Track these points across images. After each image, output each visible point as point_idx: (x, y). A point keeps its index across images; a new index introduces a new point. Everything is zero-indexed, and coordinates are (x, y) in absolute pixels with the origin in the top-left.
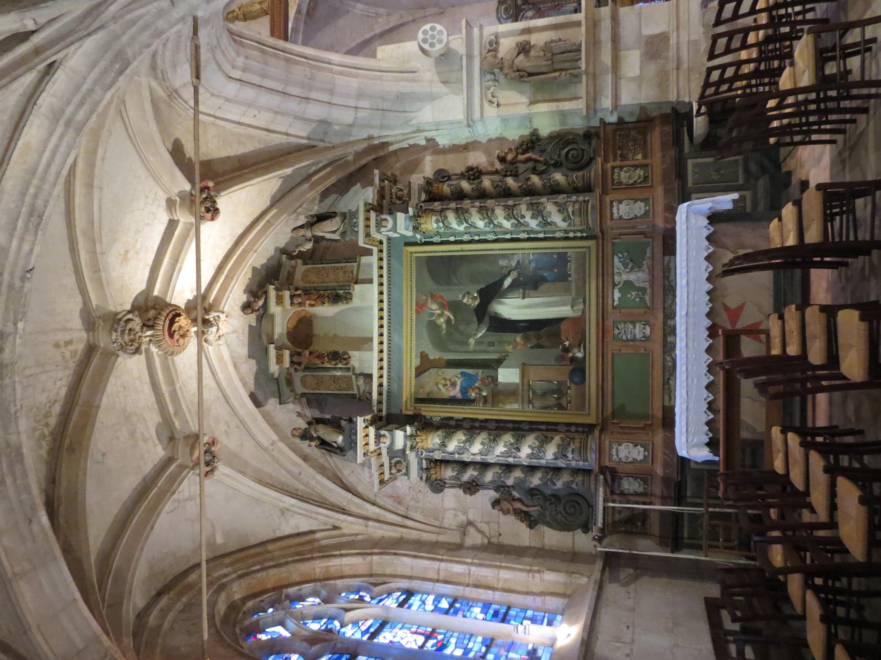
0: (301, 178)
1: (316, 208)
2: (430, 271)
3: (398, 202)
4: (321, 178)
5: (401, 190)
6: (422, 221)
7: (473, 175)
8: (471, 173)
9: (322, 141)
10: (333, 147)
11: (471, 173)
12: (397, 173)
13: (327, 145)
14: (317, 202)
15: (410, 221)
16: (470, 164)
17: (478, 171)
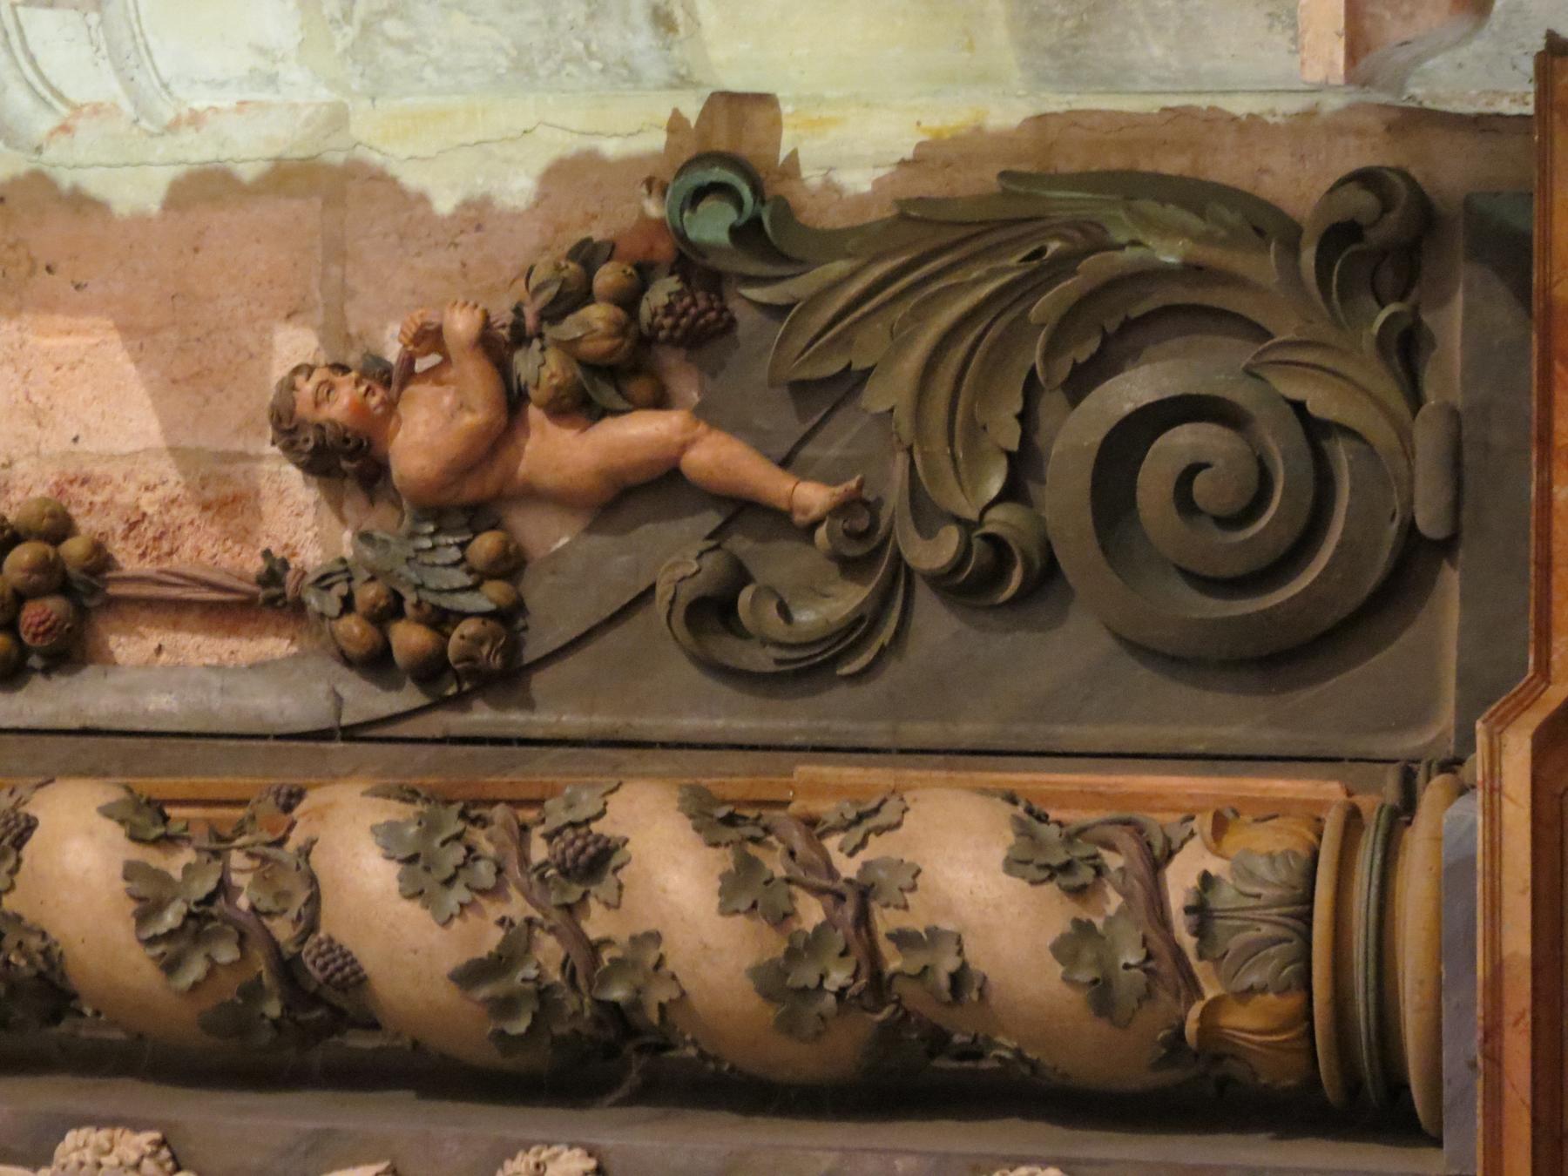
17: (54, 579)
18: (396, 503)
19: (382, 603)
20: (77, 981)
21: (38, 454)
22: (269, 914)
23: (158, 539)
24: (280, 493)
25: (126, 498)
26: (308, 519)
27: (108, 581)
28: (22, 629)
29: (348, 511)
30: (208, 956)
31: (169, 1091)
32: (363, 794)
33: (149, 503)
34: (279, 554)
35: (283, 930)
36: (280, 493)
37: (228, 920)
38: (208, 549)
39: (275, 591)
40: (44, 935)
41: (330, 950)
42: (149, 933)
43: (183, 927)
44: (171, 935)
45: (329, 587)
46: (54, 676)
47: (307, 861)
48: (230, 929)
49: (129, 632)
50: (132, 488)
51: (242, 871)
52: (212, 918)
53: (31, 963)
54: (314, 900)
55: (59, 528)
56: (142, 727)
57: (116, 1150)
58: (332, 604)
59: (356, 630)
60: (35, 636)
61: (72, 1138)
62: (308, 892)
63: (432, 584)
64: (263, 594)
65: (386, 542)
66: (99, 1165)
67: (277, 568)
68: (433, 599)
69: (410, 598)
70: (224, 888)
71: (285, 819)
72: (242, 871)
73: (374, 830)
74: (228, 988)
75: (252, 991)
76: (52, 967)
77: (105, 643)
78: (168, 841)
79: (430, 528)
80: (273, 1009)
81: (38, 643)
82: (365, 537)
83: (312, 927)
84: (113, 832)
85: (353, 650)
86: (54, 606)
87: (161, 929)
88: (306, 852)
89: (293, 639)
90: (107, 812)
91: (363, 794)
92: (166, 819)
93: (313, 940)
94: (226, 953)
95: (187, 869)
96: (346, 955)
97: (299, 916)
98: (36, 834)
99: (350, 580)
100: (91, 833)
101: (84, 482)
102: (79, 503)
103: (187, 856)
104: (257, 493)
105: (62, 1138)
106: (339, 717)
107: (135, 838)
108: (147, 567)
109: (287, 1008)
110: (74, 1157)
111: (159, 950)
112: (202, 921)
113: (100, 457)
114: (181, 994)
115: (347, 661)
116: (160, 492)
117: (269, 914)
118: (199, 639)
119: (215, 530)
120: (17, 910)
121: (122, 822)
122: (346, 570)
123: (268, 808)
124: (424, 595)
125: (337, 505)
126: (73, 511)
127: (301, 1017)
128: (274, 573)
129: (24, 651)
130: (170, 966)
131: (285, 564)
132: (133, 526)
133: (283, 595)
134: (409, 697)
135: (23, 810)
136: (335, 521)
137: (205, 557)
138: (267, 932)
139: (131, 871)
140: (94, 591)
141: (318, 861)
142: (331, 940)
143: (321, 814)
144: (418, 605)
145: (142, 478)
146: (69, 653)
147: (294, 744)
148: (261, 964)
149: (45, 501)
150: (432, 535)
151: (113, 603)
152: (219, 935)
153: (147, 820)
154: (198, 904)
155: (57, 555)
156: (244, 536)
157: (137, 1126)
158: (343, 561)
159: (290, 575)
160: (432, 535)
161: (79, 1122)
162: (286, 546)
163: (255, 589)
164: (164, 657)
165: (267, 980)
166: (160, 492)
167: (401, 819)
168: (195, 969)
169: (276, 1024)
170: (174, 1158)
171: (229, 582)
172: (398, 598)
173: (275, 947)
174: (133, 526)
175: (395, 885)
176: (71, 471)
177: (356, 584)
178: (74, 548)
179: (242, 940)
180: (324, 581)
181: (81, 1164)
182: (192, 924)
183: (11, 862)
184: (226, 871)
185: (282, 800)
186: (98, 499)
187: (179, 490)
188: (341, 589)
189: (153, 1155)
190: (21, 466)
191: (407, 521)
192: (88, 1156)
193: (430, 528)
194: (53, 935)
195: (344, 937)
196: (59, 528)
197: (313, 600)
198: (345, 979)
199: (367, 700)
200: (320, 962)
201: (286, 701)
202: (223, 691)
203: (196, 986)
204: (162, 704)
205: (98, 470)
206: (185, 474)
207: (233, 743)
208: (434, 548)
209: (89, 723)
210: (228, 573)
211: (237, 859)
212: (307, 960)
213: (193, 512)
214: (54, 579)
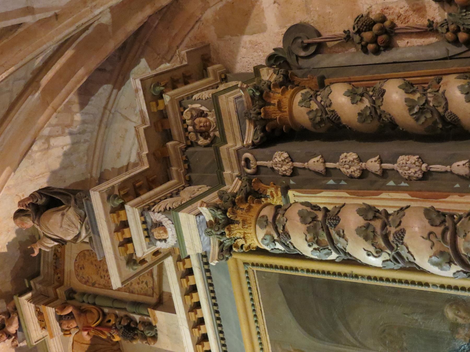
0: (22, 83)
1: (78, 117)
2: (290, 304)
3: (202, 141)
4: (58, 75)
5: (202, 114)
6: (237, 231)
7: (374, 40)
8: (367, 35)
9: (29, 10)
10: (56, 16)
11: (367, 35)
12: (211, 34)
13: (39, 16)
14: (76, 107)
15: (209, 234)
16: (364, 10)
17: (384, 31)
18: (456, 5)
19: (455, 29)
20: (397, 123)
21: (377, 4)
22: (437, 106)
23: (404, 19)
24: (430, 6)
25: (397, 11)
26: (437, 11)
27: (395, 30)
28: (378, 42)
29: (446, 8)
30: (425, 117)
31: (419, 144)
32: (455, 78)
33: (402, 11)
34: (431, 20)
35: (441, 110)
36: (430, 6)
37: (428, 109)
38: (416, 20)
39: (431, 28)
40: (390, 115)
41: (451, 114)
42: (412, 113)
43: (419, 111)
44: (416, 113)
45: (443, 26)
46: (386, 51)
47: (444, 95)
48: (429, 110)
49: (401, 39)
50: (398, 9)
51: (430, 97)
52: (425, 109)
53: (388, 120)
54: (447, 104)
55: (383, 19)
56: (406, 60)
57: (410, 160)
58: (444, 31)
59: (450, 35)
60: (381, 43)
61: (401, 158)
62: (445, 102)
63: (466, 24)
64: (429, 29)
65: (455, 15)
66: (407, 163)
67: (431, 23)
68: (467, 27)
69: (462, 28)
70: (427, 102)
71: (438, 86)
72: (430, 97)
73: (458, 87)
74: (430, 123)
75: (435, 123)
76: (392, 120)
77: (396, 42)
78: (414, 92)
79: (464, 11)
80: (440, 126)
81: (382, 45)
82: (450, 14)
83: (447, 109)
84: (401, 91)
85: (450, 40)
86: (384, 37)
87: (414, 112)
88: (444, 93)
89: (437, 37)
90: (400, 87)
91: (455, 78)
92: (414, 87)
93: (447, 112)
94: (429, 116)
95: (419, 98)
96: (455, 115)
97: (444, 107)
98: (386, 93)
99: (447, 24)
100: (397, 92)
101: (387, 9)
102: (387, 13)
103: (418, 95)
104: (425, 6)
105: (398, 158)
106: (448, 54)
107: (407, 92)
108: (403, 25)
109: (443, 126)
110: (401, 162)
111: (414, 116)
112: (422, 110)
113: (390, 3)
114: (421, 125)
115: (449, 42)
116: (404, 9)
117: (437, 106)
118: (416, 39)
119: (417, 16)
120: (384, 110)
121: (403, 89)
122: (447, 22)
123: (435, 83)
124: (464, 26)
125: (443, 7)
126: (386, 15)
127: (447, 127)
128: (431, 23)
129: (379, 47)
130: (417, 120)
131: (433, 22)
132: (399, 17)
133: (433, 29)
134: (464, 48)
135: (382, 88)
136: (443, 11)
137: (415, 22)
138: (437, 110)
139: (407, 100)
140: (392, 32)
141: (447, 95)
142: (451, 112)
143: (446, 84)
144: (464, 28)
145: (400, 6)
146: (389, 46)
147: (439, 61)
148: (436, 117)
149: (379, 14)
150: (465, 12)
151: (396, 34)
152: (427, 112)
153: (409, 87)
154: (421, 106)
155: (384, 26)
156: (423, 16)
157: (414, 155)
158: (446, 20)
159: (434, 24)
160: (465, 12)
161: (402, 154)
162: (433, 17)
163: (427, 28)
164: (409, 44)
165: (438, 121)
166: (404, 9)
167: (464, 84)
168: (423, 120)
169: (441, 129)
170: (422, 161)
171: (421, 27)
172: (458, 27)
173: (439, 113)
174: (399, 17)
175: (464, 100)
176: (384, 7)
177: (449, 25)
178: (387, 23)
179: (432, 113)
180: (442, 25)
181: (403, 163)
182: (421, 111)
183: (381, 100)
184: (427, 98)
185: (437, 81)
186: (391, 12)
187: (408, 8)
188: (446, 27)
189: (418, 161)
190: (374, 7)
191: (459, 10)
192: (404, 162)
193: (464, 11)
194: (392, 115)
195: (454, 111)
196: (383, 19)
197: (440, 29)
198: (455, 120)
199: (454, 50)
200: (449, 117)
201: (437, 52)
202: (423, 51)
203: (423, 123)
204: (409, 56)
205: (390, 6)
206: (408, 4)
207: (426, 62)
208: (466, 15)
209: (395, 61)
210: (420, 25)
211: (429, 95)
212: (446, 117)
213: (411, 13)
214: (384, 31)
